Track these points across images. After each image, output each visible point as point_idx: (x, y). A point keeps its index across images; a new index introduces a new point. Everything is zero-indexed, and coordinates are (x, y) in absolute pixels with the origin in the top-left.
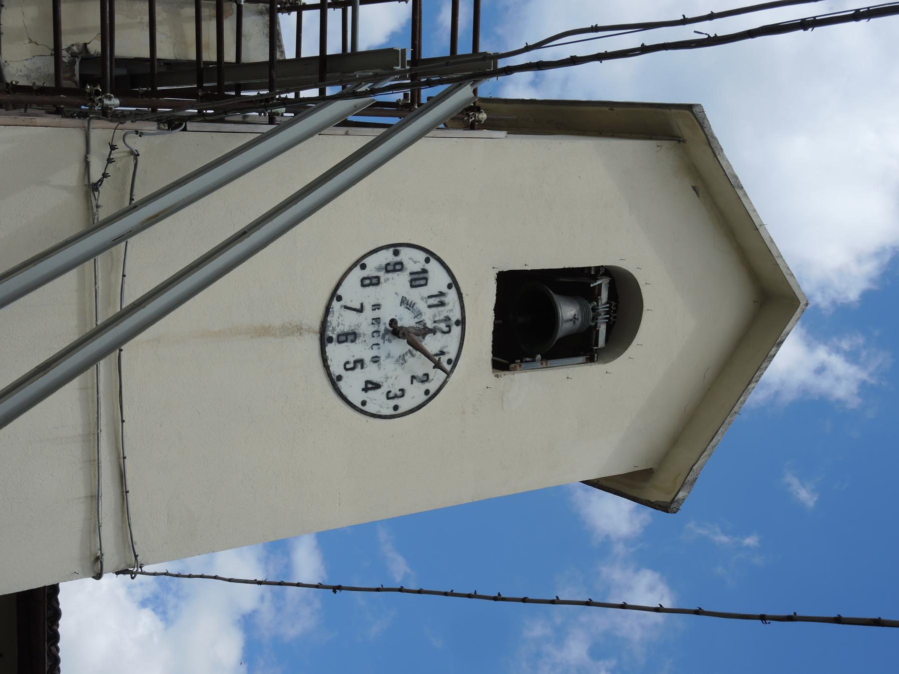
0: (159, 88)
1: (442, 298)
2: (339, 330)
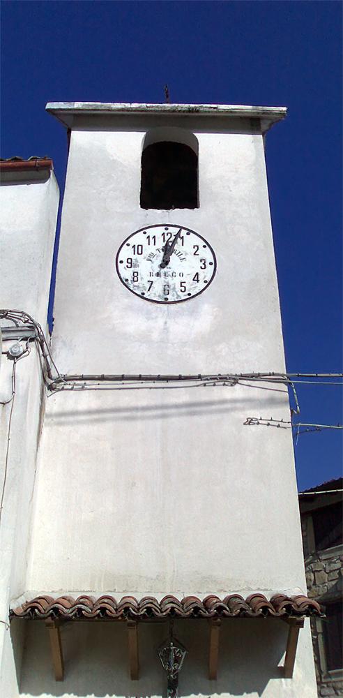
0: (49, 106)
1: (151, 238)
2: (162, 294)
